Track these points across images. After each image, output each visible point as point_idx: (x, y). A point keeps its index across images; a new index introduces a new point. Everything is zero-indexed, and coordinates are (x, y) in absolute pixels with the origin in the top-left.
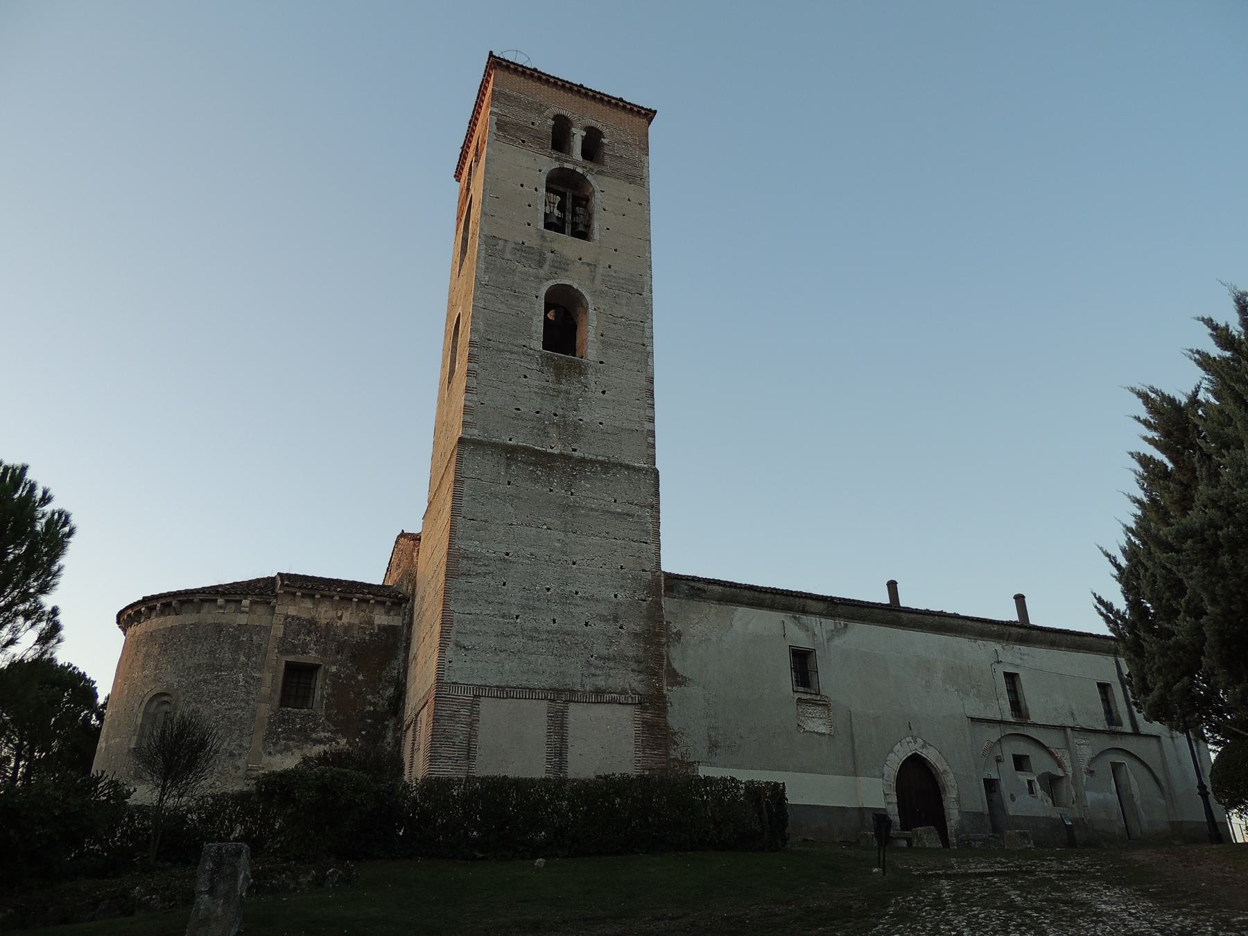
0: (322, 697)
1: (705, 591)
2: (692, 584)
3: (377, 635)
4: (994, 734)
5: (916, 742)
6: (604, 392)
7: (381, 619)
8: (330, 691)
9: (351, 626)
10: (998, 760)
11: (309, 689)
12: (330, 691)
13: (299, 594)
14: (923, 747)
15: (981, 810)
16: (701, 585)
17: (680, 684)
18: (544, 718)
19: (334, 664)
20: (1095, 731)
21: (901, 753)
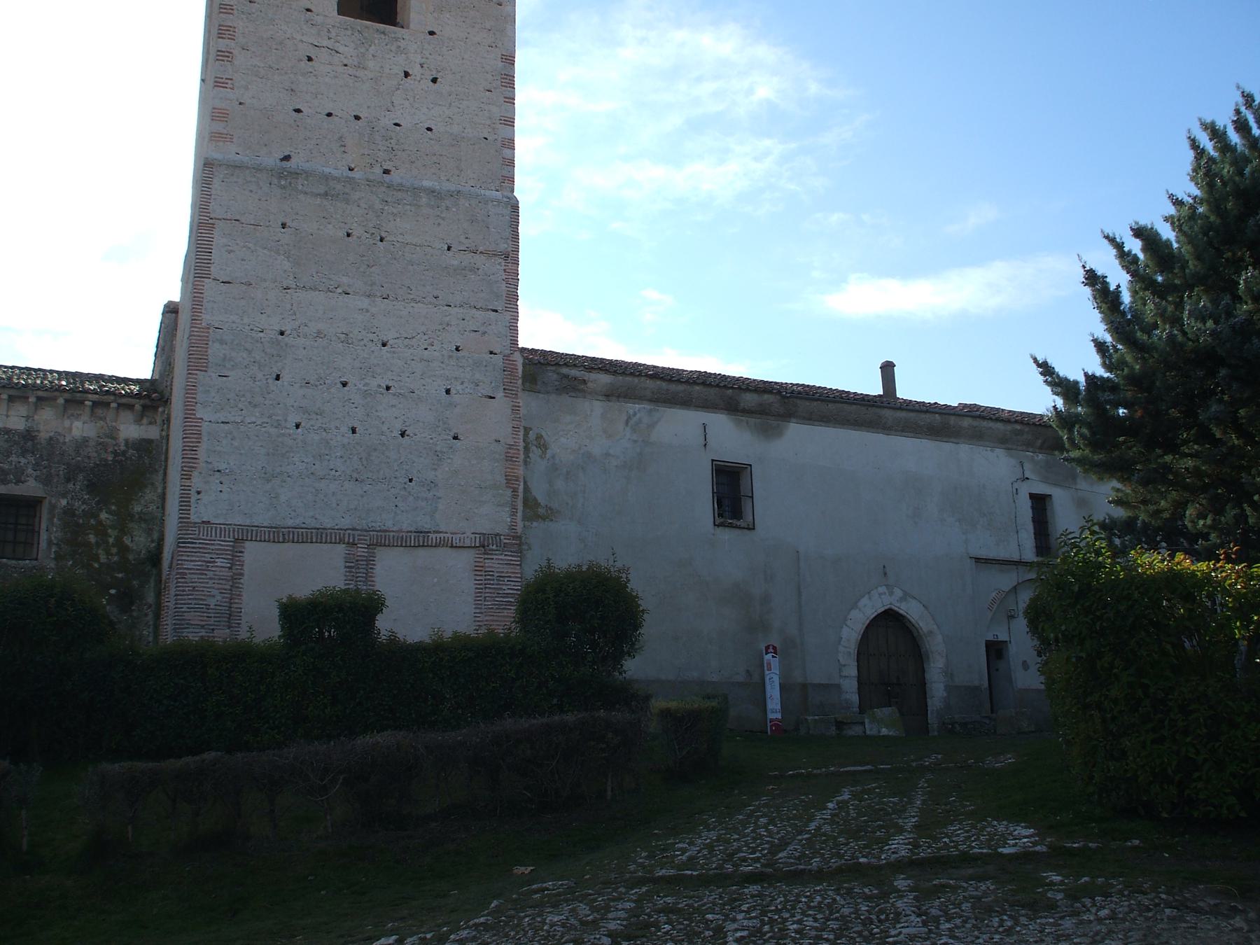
0: (50, 543)
1: (584, 382)
2: (565, 370)
3: (124, 453)
4: (1007, 580)
5: (891, 593)
6: (434, 80)
7: (130, 429)
8: (60, 534)
9: (86, 440)
10: (1011, 617)
11: (33, 532)
12: (60, 534)
13: (114, 405)
14: (902, 599)
15: (976, 683)
16: (574, 372)
17: (544, 518)
18: (340, 563)
19: (64, 496)
20: (1026, 564)
21: (870, 608)
